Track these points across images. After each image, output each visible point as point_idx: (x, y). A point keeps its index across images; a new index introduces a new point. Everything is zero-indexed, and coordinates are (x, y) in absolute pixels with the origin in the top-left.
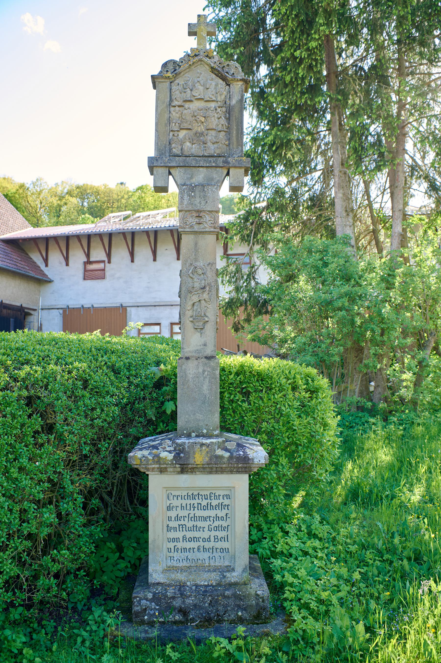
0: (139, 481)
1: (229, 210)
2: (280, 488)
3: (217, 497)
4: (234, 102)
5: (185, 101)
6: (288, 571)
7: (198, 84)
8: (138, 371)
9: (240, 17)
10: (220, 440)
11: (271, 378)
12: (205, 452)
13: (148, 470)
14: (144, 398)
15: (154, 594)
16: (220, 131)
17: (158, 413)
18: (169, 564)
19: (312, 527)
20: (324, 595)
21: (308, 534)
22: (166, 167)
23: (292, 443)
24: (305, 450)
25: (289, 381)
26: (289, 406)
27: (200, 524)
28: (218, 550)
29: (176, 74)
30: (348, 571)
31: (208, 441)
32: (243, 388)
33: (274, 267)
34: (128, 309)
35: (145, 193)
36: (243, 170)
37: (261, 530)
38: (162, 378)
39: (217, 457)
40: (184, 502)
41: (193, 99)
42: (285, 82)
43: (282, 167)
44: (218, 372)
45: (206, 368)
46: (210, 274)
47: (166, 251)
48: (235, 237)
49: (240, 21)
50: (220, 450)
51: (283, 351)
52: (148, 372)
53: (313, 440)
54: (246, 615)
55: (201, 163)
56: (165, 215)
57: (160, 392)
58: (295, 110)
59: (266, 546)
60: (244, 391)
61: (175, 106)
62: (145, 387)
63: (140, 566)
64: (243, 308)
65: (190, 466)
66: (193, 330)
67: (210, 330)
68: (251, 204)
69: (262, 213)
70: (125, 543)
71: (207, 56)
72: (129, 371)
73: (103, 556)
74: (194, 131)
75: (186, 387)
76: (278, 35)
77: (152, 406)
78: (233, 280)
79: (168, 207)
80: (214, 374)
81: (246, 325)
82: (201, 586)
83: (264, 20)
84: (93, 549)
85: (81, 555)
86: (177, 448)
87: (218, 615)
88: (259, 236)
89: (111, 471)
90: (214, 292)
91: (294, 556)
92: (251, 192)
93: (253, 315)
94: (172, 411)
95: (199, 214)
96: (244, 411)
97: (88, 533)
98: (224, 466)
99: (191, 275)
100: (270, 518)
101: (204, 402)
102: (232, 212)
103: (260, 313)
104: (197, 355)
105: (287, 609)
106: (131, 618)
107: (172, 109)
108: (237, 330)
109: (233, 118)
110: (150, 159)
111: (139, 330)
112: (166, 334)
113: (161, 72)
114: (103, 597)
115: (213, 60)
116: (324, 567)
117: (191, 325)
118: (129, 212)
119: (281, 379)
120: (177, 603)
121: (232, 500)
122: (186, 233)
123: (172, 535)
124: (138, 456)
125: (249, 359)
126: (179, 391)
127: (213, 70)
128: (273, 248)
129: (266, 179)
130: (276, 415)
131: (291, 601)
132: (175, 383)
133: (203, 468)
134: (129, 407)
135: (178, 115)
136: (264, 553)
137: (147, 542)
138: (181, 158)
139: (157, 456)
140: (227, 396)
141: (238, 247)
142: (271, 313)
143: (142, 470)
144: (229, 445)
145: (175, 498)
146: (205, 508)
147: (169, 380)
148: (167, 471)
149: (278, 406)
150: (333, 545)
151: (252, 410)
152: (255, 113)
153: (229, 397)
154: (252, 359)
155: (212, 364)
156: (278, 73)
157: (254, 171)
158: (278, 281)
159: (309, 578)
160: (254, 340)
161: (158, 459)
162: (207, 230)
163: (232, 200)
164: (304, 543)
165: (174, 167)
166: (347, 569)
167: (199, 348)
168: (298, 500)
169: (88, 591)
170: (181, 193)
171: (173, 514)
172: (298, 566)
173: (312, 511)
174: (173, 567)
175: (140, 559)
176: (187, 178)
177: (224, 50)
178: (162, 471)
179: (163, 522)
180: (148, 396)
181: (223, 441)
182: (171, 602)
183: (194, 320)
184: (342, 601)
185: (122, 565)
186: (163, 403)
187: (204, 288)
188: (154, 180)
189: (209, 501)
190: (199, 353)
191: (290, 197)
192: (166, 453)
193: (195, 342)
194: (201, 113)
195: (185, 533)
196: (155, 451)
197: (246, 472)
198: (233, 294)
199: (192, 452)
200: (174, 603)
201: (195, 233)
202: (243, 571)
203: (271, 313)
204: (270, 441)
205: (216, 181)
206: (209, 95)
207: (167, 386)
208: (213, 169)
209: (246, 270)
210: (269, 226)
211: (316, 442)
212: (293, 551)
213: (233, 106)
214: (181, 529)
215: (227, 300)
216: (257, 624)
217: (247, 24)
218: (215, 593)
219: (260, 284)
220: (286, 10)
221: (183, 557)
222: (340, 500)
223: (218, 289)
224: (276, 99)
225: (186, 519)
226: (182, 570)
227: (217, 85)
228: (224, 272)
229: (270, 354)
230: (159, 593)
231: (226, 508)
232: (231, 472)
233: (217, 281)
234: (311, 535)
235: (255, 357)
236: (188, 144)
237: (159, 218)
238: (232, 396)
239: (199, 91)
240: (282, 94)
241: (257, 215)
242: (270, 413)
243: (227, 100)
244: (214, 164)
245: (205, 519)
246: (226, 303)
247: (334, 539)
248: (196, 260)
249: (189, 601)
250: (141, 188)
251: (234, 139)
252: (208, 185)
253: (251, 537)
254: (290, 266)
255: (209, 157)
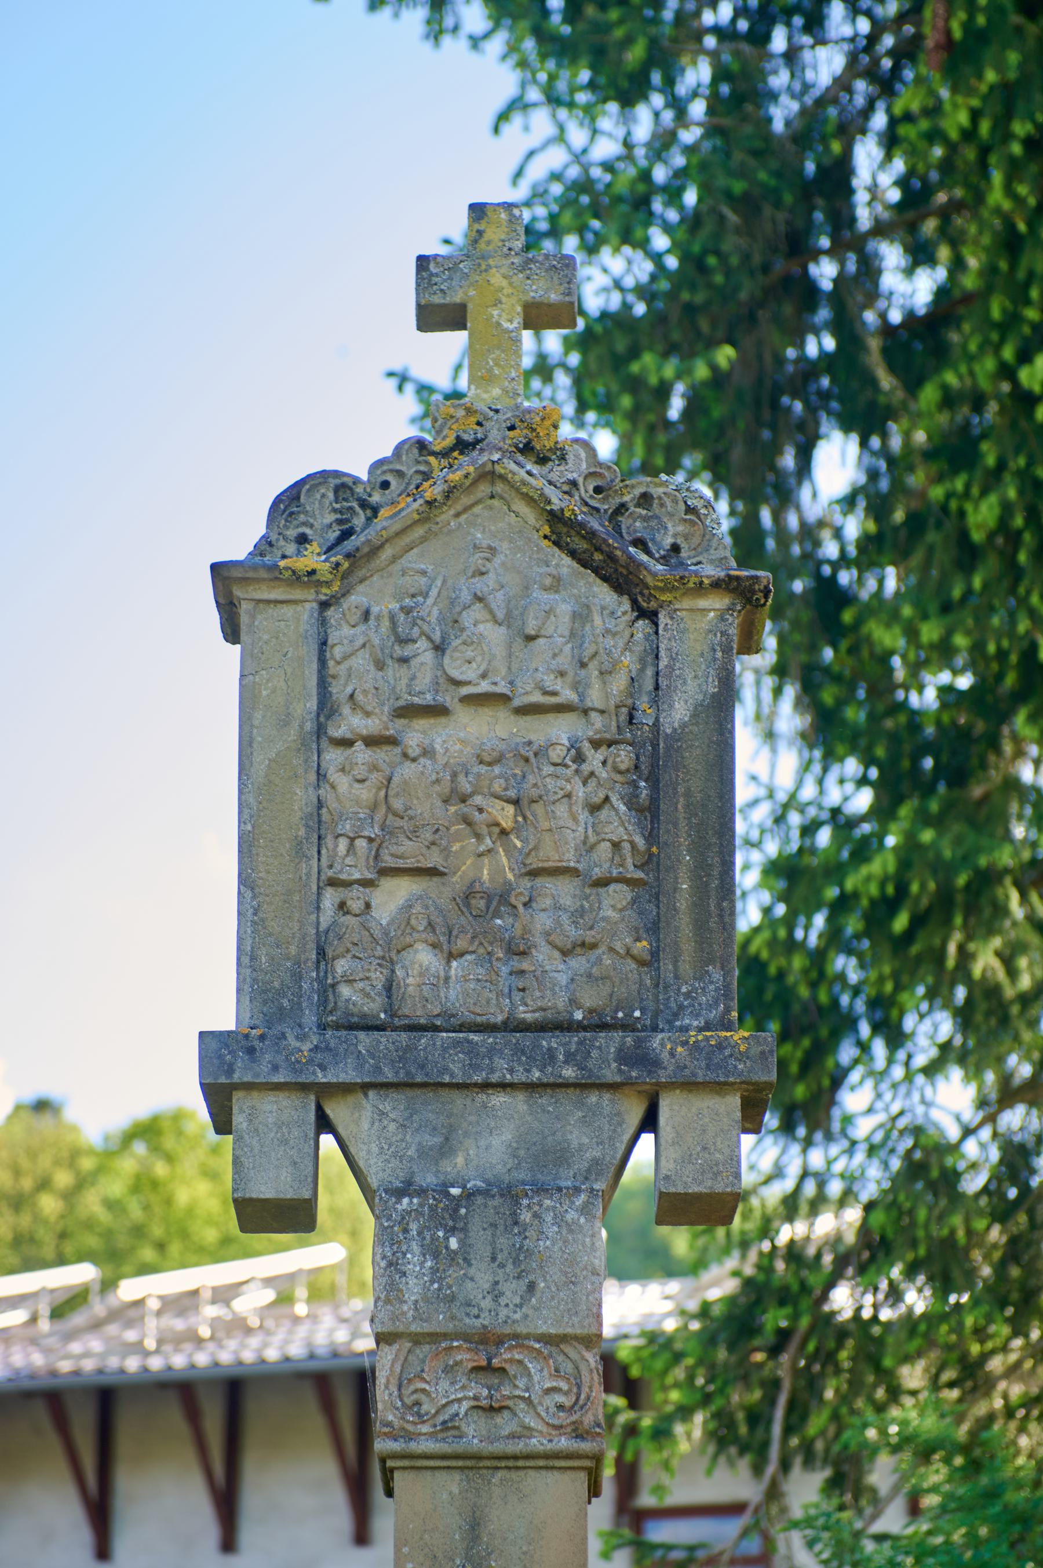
4: (679, 712)
5: (408, 712)
7: (477, 612)
9: (704, 166)
16: (603, 883)
22: (304, 1088)
29: (354, 558)
35: (170, 1158)
36: (734, 1101)
41: (448, 698)
42: (964, 535)
43: (945, 1026)
48: (679, 1429)
49: (705, 190)
55: (501, 1063)
58: (1019, 697)
61: (346, 743)
71: (527, 449)
74: (457, 881)
76: (920, 255)
83: (838, 176)
88: (817, 1423)
107: (333, 756)
109: (677, 809)
110: (214, 1048)
113: (265, 545)
115: (559, 473)
118: (83, 1273)
127: (561, 529)
128: (896, 1490)
129: (855, 1098)
135: (365, 793)
138: (384, 1039)
152: (789, 718)
156: (916, 479)
165: (345, 1089)
170: (390, 1238)
176: (423, 1153)
177: (619, 362)
194: (496, 778)
201: (470, 1462)
205: (581, 1165)
206: (541, 672)
213: (676, 737)
217: (748, 205)
220: (975, 115)
224: (911, 633)
227: (581, 616)
236: (424, 957)
237: (250, 1303)
239: (483, 654)
240: (947, 608)
241: (805, 1303)
243: (643, 703)
244: (569, 1073)
250: (148, 1131)
251: (684, 924)
252: (541, 1190)
255: (541, 1028)
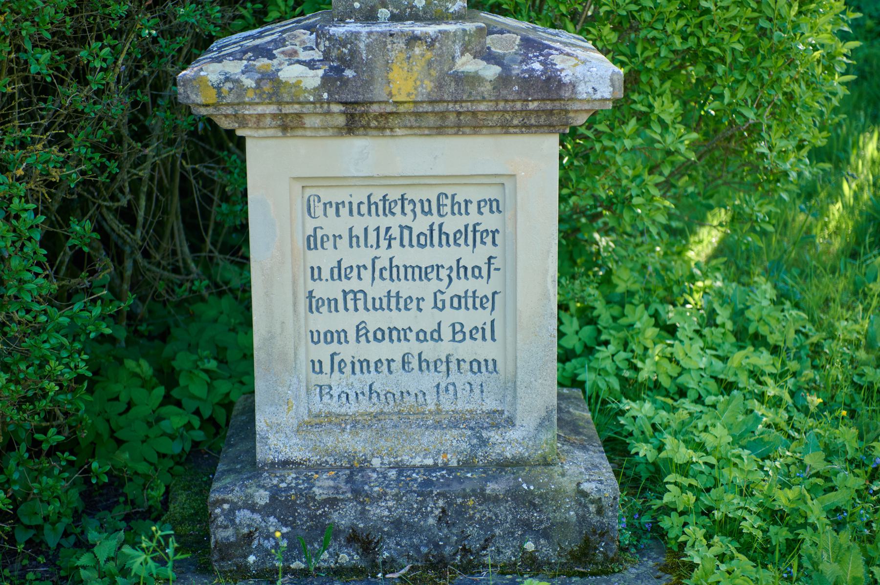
0: (217, 175)
2: (654, 191)
3: (461, 207)
6: (675, 434)
10: (470, 26)
12: (423, 63)
13: (243, 121)
15: (275, 493)
18: (318, 406)
19: (748, 314)
20: (784, 499)
21: (735, 334)
23: (693, 56)
24: (737, 75)
27: (407, 288)
28: (465, 366)
30: (861, 437)
31: (432, 29)
37: (593, 321)
39: (461, 79)
40: (359, 224)
50: (468, 56)
53: (765, 44)
54: (547, 551)
59: (608, 365)
63: (226, 425)
65: (375, 108)
70: (183, 361)
73: (117, 399)
82: (413, 468)
84: (83, 369)
85: (46, 384)
86: (334, 53)
87: (466, 551)
89: (127, 139)
91: (692, 395)
97: (64, 320)
98: (483, 107)
100: (621, 288)
105: (671, 535)
106: (209, 563)
114: (120, 511)
116: (783, 424)
120: (344, 517)
121: (508, 214)
123: (324, 321)
124: (212, 77)
131: (682, 514)
133: (417, 114)
136: (602, 385)
137: (248, 356)
139: (272, 77)
143: (225, 124)
144: (495, 44)
145: (331, 211)
146: (425, 240)
148: (302, 127)
150: (814, 367)
159: (737, 451)
161: (273, 87)
164: (724, 359)
166: (854, 431)
168: (707, 239)
169: (74, 494)
171: (325, 259)
172: (706, 420)
173: (748, 274)
174: (329, 415)
175: (228, 405)
178: (287, 125)
179: (294, 282)
181: (480, 30)
182: (325, 515)
184: (839, 517)
185: (176, 420)
189: (436, 219)
192: (299, 69)
195: (362, 315)
196: (262, 62)
197: (550, 128)
199: (380, 63)
200: (335, 516)
202: (542, 425)
204: (623, 48)
211: (772, 51)
212: (690, 381)
214: (351, 305)
216: (583, 575)
218: (456, 487)
221: (358, 386)
222: (837, 244)
225: (366, 274)
226: (355, 423)
230: (289, 488)
231: (488, 240)
232: (505, 128)
234: (747, 336)
245: (424, 273)
247: (817, 350)
249: (379, 511)
253: (564, 342)
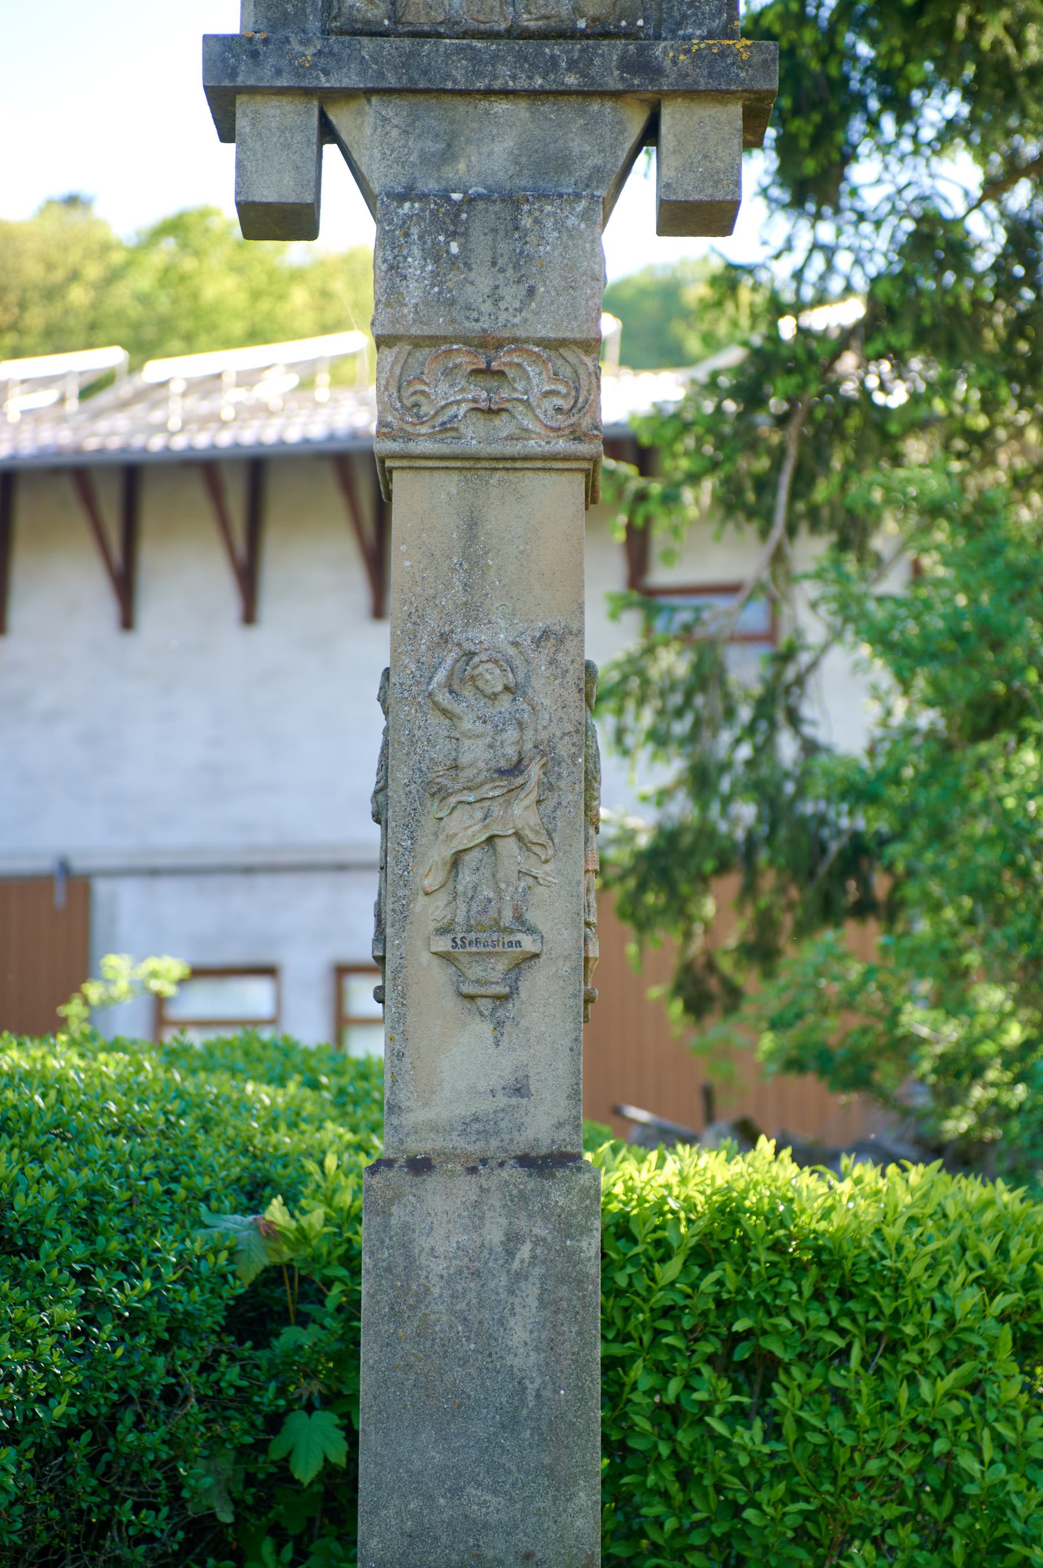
1: (651, 349)
8: (139, 1235)
11: (897, 1282)
14: (171, 1396)
17: (250, 1480)
25: (1002, 1302)
26: (1001, 1444)
32: (735, 1339)
33: (903, 656)
34: (102, 888)
38: (274, 1275)
44: (591, 1246)
45: (522, 1224)
46: (551, 694)
47: (314, 567)
48: (688, 494)
51: (959, 1124)
52: (197, 1244)
55: (504, 70)
56: (299, 370)
57: (262, 1356)
60: (742, 1353)
62: (180, 1327)
64: (732, 883)
66: (450, 1002)
67: (547, 1005)
68: (777, 308)
69: (836, 356)
72: (88, 1240)
75: (410, 1329)
77: (215, 1442)
78: (681, 728)
79: (325, 329)
80: (572, 1257)
81: (748, 979)
88: (822, 491)
90: (571, 795)
92: (778, 243)
93: (787, 922)
94: (329, 1471)
95: (488, 357)
96: (740, 1473)
99: (444, 698)
101: (511, 1423)
102: (671, 356)
103: (827, 911)
104: (476, 1148)
108: (697, 1005)
110: (220, 53)
111: (159, 1002)
112: (309, 1028)
117: (439, 975)
118: (110, 357)
119: (954, 1284)
122: (416, 462)
125: (766, 1172)
126: (369, 1352)
129: (864, 171)
130: (927, 1502)
132: (351, 1309)
134: (81, 1446)
138: (388, 45)
140: (646, 1382)
141: (708, 553)
142: (891, 911)
147: (312, 1291)
149: (940, 1446)
151: (782, 1472)
153: (651, 1392)
154: (787, 1169)
155: (558, 1198)
157: (796, 125)
158: (931, 735)
160: (794, 1064)
162: (534, 446)
163: (668, 292)
165: (349, 94)
167: (485, 1106)
176: (425, 159)
180: (192, 1380)
183: (461, 945)
186: (275, 1422)
187: (517, 768)
188: (240, 165)
190: (484, 1134)
191: (997, 268)
193: (461, 1071)
198: (682, 808)
201: (469, 463)
203: (891, 911)
207: (304, 1320)
208: (569, 107)
209: (746, 671)
210: (880, 435)
215: (643, 841)
219: (828, 750)
223: (591, 779)
228: (634, 680)
229: (888, 1139)
233: (586, 733)
235: (804, 1158)
238: (674, 1386)
242: (893, 1489)
244: (571, 80)
246: (641, 856)
248: (472, 612)
250: (175, 227)
252: (542, 196)
254: (997, 646)
